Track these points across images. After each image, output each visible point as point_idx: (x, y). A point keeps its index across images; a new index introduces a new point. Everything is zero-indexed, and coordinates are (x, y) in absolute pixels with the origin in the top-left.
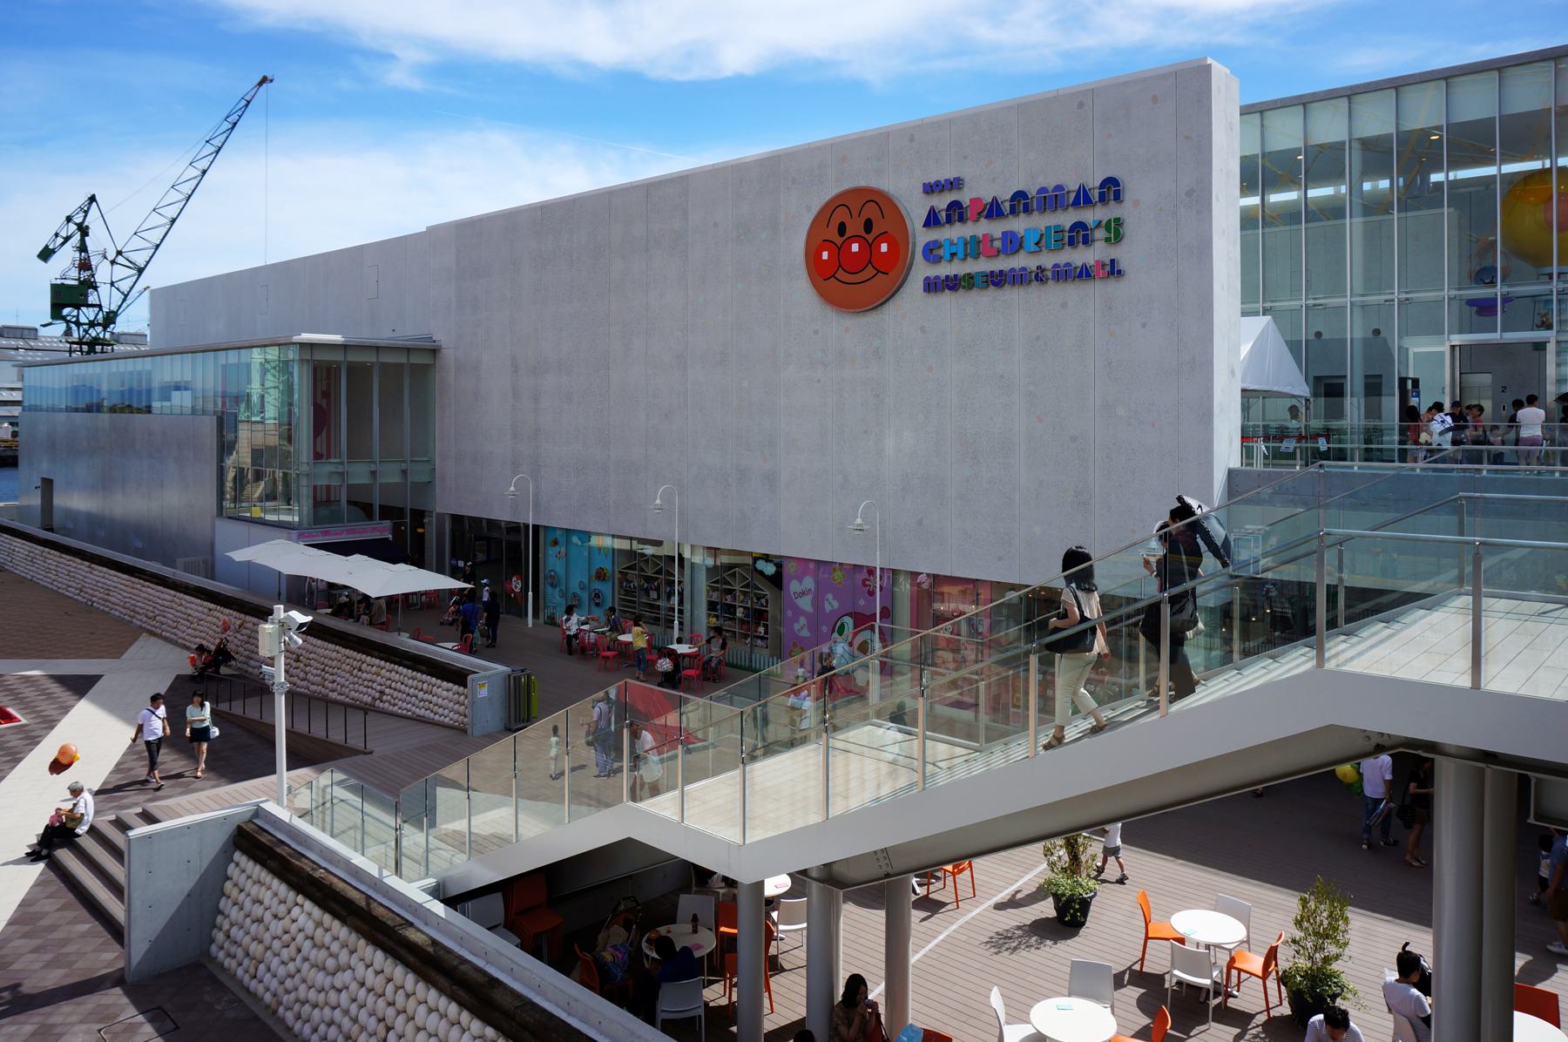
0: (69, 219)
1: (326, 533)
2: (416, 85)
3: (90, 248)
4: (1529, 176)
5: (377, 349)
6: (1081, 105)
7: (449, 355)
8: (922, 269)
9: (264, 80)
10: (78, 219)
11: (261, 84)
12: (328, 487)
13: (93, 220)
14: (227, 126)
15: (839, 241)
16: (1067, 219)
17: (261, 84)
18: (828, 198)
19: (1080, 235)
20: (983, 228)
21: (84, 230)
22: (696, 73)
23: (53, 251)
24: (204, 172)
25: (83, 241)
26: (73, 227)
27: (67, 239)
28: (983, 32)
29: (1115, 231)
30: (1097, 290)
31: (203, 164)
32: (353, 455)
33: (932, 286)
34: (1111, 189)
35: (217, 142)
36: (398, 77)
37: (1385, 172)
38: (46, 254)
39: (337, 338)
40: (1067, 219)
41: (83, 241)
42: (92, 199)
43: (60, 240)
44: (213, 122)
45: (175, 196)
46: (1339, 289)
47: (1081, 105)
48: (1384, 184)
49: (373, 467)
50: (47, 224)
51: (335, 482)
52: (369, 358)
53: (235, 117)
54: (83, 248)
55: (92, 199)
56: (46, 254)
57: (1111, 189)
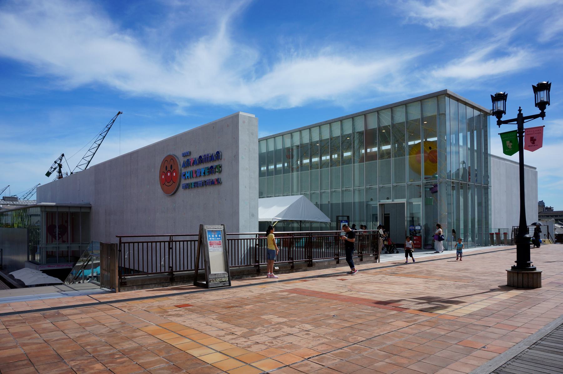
0: (55, 162)
1: (49, 266)
2: (185, 114)
3: (62, 172)
4: (415, 145)
5: (69, 207)
6: (214, 127)
7: (93, 208)
8: (184, 182)
9: (119, 113)
10: (58, 162)
11: (118, 114)
12: (52, 252)
13: (63, 163)
14: (107, 129)
15: (166, 172)
16: (209, 165)
17: (118, 114)
18: (164, 157)
19: (211, 170)
20: (195, 168)
21: (60, 166)
22: (281, 107)
23: (50, 173)
24: (99, 145)
25: (60, 170)
26: (57, 165)
27: (55, 169)
28: (381, 89)
29: (219, 169)
30: (210, 189)
31: (99, 142)
32: (73, 241)
33: (187, 186)
34: (218, 156)
35: (104, 135)
36: (179, 111)
37: (387, 143)
38: (48, 174)
39: (54, 204)
40: (209, 165)
41: (60, 170)
42: (63, 155)
43: (53, 169)
44: (102, 127)
45: (90, 153)
46: (389, 182)
47: (214, 127)
48: (388, 147)
49: (79, 245)
50: (48, 164)
51: (54, 250)
52: (78, 210)
53: (109, 126)
54: (60, 172)
55: (63, 155)
56: (48, 174)
57: (218, 156)
